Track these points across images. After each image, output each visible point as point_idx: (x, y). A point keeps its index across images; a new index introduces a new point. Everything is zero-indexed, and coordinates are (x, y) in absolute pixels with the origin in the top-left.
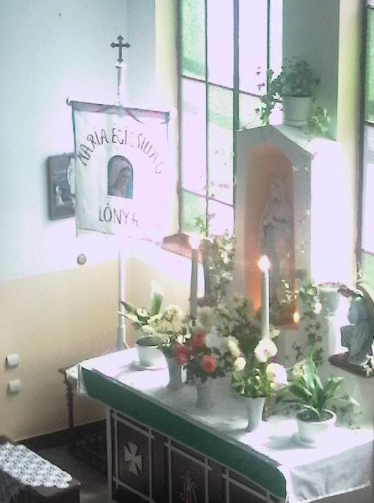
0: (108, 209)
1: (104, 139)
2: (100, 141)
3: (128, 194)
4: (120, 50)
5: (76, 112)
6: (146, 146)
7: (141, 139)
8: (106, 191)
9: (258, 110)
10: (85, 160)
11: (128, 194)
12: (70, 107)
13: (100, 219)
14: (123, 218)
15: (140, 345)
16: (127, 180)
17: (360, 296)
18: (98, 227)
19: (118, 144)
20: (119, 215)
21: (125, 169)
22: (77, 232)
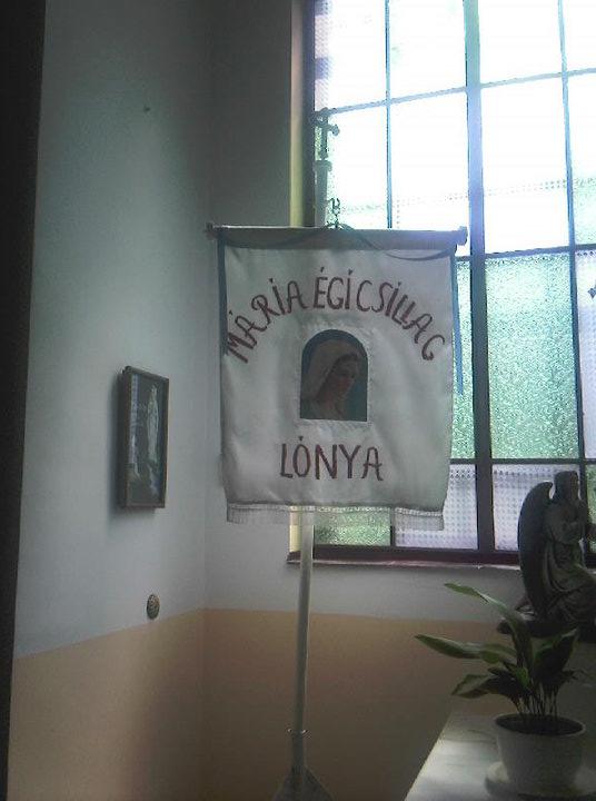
0: (301, 449)
1: (294, 301)
2: (285, 306)
3: (355, 409)
4: (557, 76)
5: (228, 251)
6: (401, 302)
7: (388, 292)
8: (295, 409)
9: (399, 284)
10: (241, 349)
11: (355, 409)
12: (214, 241)
13: (283, 474)
14: (342, 467)
15: (502, 726)
16: (352, 381)
17: (543, 709)
18: (270, 493)
19: (328, 310)
20: (330, 461)
21: (345, 358)
22: (228, 508)
